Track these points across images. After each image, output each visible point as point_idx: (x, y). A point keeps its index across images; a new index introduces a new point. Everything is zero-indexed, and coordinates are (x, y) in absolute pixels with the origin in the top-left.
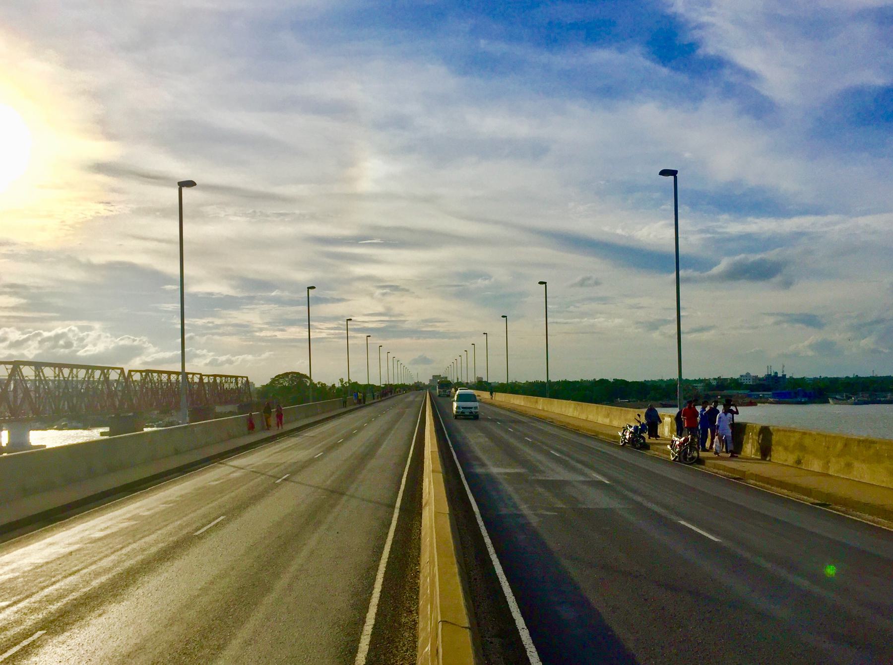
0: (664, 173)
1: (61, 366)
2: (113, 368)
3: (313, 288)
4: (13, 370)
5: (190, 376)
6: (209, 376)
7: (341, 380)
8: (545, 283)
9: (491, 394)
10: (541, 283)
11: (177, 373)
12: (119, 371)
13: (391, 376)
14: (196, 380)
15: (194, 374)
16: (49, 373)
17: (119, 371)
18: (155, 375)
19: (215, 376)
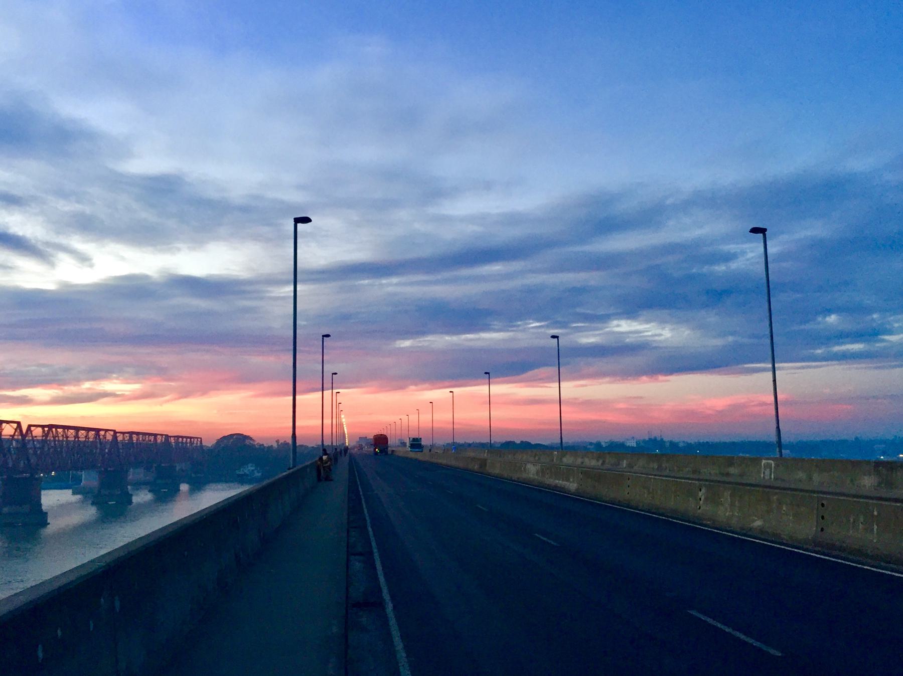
2: (8, 422)
6: (123, 433)
12: (15, 425)
15: (106, 431)
18: (60, 430)
19: (131, 433)
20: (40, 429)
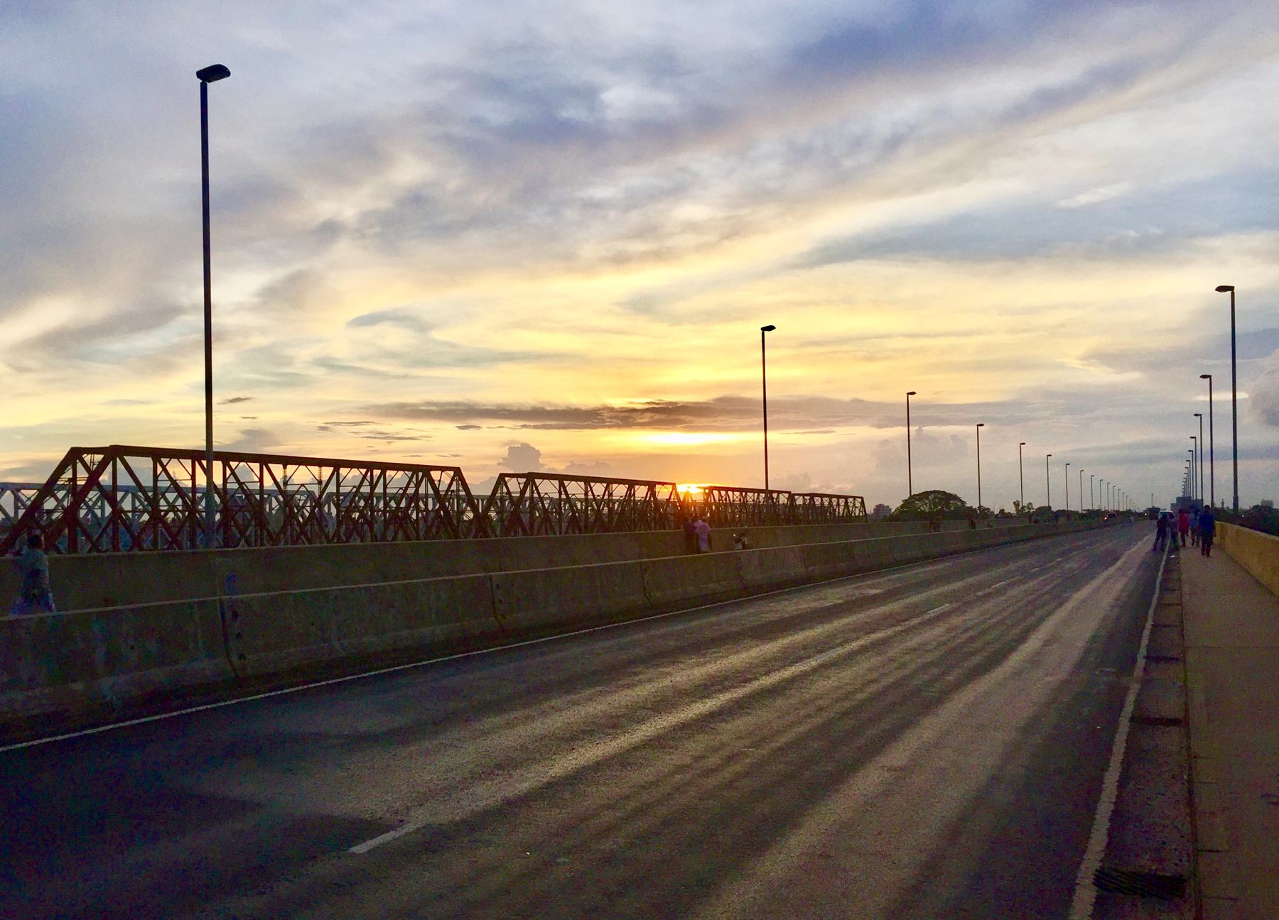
0: (1221, 289)
1: (588, 480)
3: (913, 393)
4: (526, 485)
5: (775, 495)
6: (804, 495)
7: (1016, 504)
8: (1231, 289)
9: (285, 468)
10: (1204, 377)
11: (759, 491)
12: (452, 473)
13: (1087, 493)
14: (783, 499)
15: (779, 492)
16: (576, 489)
17: (452, 473)
18: (750, 494)
19: (812, 496)
20: (737, 494)
